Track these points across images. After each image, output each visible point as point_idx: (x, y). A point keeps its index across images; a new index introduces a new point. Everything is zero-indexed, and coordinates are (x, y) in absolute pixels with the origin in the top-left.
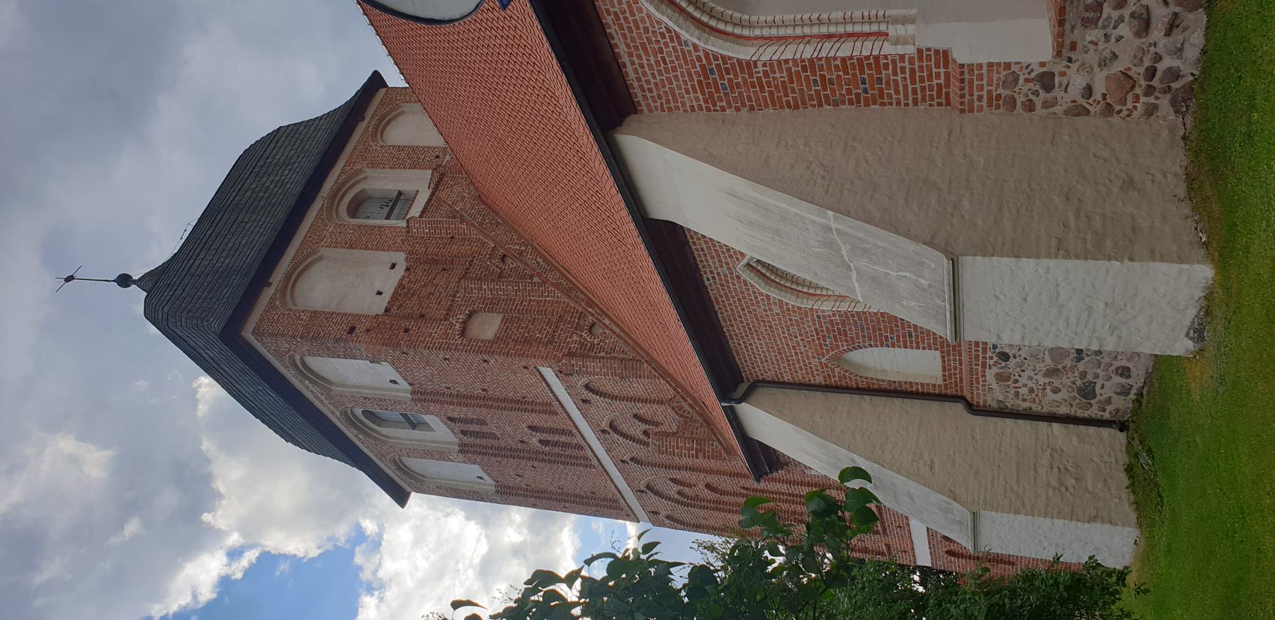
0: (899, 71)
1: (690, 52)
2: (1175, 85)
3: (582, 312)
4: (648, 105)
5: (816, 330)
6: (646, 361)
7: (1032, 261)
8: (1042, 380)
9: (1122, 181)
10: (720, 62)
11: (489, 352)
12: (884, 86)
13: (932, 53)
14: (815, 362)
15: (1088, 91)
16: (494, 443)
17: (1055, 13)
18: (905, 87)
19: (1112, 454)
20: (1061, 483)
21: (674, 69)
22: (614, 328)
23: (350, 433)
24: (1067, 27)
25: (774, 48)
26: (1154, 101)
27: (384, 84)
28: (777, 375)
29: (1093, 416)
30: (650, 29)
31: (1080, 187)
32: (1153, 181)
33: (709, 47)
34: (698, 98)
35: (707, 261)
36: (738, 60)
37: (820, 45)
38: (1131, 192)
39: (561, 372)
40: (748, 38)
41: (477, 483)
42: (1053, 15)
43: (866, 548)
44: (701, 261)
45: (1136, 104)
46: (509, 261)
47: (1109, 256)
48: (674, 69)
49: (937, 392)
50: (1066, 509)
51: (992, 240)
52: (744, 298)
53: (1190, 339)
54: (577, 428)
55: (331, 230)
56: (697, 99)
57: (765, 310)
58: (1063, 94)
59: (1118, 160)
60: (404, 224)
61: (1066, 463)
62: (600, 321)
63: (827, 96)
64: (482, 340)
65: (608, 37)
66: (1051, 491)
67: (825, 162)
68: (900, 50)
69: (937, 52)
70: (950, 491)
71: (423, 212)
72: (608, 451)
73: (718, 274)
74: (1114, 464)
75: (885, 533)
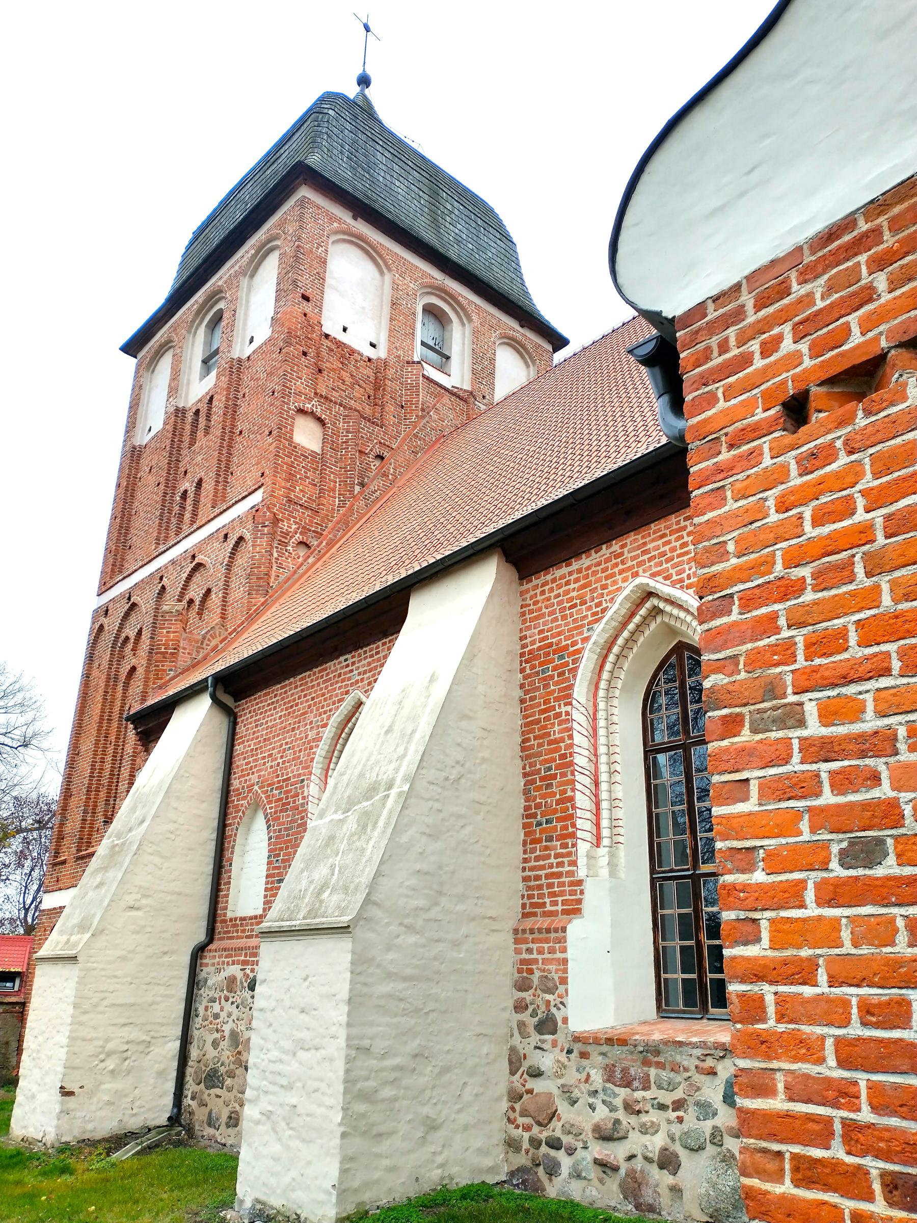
0: (560, 860)
1: (581, 633)
2: (541, 1171)
3: (322, 534)
4: (527, 591)
5: (289, 779)
6: (267, 600)
7: (344, 1019)
8: (227, 1028)
9: (434, 1117)
10: (571, 666)
11: (280, 437)
12: (544, 844)
13: (578, 896)
14: (254, 778)
15: (536, 1074)
16: (186, 444)
17: (620, 1034)
18: (542, 868)
19: (142, 1110)
20: (109, 1054)
21: (564, 618)
22: (304, 567)
23: (200, 296)
24: (605, 1048)
25: (585, 724)
26: (524, 1147)
27: (556, 349)
28: (241, 737)
29: (187, 1086)
30: (605, 591)
31: (430, 1068)
32: (434, 1153)
33: (586, 654)
34: (535, 644)
35: (365, 658)
36: (573, 685)
37: (587, 773)
38: (422, 1129)
39: (257, 511)
40: (595, 695)
41: (145, 425)
42: (619, 1031)
43: (63, 839)
44: (365, 652)
45: (521, 1128)
46: (378, 463)
47: (348, 1109)
48: (564, 618)
49: (219, 912)
50: (78, 1060)
51: (371, 971)
52: (325, 700)
53: (253, 1205)
54: (198, 528)
55: (411, 285)
56: (533, 643)
57: (311, 723)
58: (533, 1044)
59: (460, 1111)
60: (416, 359)
61: (133, 1058)
62: (312, 553)
63: (533, 782)
64: (292, 430)
65: (598, 546)
66: (101, 1043)
67: (463, 781)
68: (582, 861)
69: (579, 901)
70: (104, 930)
71: (428, 378)
72: (173, 562)
73: (352, 671)
74: (131, 1112)
75: (78, 858)
